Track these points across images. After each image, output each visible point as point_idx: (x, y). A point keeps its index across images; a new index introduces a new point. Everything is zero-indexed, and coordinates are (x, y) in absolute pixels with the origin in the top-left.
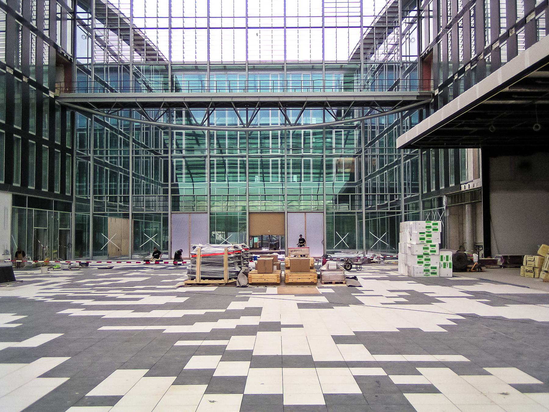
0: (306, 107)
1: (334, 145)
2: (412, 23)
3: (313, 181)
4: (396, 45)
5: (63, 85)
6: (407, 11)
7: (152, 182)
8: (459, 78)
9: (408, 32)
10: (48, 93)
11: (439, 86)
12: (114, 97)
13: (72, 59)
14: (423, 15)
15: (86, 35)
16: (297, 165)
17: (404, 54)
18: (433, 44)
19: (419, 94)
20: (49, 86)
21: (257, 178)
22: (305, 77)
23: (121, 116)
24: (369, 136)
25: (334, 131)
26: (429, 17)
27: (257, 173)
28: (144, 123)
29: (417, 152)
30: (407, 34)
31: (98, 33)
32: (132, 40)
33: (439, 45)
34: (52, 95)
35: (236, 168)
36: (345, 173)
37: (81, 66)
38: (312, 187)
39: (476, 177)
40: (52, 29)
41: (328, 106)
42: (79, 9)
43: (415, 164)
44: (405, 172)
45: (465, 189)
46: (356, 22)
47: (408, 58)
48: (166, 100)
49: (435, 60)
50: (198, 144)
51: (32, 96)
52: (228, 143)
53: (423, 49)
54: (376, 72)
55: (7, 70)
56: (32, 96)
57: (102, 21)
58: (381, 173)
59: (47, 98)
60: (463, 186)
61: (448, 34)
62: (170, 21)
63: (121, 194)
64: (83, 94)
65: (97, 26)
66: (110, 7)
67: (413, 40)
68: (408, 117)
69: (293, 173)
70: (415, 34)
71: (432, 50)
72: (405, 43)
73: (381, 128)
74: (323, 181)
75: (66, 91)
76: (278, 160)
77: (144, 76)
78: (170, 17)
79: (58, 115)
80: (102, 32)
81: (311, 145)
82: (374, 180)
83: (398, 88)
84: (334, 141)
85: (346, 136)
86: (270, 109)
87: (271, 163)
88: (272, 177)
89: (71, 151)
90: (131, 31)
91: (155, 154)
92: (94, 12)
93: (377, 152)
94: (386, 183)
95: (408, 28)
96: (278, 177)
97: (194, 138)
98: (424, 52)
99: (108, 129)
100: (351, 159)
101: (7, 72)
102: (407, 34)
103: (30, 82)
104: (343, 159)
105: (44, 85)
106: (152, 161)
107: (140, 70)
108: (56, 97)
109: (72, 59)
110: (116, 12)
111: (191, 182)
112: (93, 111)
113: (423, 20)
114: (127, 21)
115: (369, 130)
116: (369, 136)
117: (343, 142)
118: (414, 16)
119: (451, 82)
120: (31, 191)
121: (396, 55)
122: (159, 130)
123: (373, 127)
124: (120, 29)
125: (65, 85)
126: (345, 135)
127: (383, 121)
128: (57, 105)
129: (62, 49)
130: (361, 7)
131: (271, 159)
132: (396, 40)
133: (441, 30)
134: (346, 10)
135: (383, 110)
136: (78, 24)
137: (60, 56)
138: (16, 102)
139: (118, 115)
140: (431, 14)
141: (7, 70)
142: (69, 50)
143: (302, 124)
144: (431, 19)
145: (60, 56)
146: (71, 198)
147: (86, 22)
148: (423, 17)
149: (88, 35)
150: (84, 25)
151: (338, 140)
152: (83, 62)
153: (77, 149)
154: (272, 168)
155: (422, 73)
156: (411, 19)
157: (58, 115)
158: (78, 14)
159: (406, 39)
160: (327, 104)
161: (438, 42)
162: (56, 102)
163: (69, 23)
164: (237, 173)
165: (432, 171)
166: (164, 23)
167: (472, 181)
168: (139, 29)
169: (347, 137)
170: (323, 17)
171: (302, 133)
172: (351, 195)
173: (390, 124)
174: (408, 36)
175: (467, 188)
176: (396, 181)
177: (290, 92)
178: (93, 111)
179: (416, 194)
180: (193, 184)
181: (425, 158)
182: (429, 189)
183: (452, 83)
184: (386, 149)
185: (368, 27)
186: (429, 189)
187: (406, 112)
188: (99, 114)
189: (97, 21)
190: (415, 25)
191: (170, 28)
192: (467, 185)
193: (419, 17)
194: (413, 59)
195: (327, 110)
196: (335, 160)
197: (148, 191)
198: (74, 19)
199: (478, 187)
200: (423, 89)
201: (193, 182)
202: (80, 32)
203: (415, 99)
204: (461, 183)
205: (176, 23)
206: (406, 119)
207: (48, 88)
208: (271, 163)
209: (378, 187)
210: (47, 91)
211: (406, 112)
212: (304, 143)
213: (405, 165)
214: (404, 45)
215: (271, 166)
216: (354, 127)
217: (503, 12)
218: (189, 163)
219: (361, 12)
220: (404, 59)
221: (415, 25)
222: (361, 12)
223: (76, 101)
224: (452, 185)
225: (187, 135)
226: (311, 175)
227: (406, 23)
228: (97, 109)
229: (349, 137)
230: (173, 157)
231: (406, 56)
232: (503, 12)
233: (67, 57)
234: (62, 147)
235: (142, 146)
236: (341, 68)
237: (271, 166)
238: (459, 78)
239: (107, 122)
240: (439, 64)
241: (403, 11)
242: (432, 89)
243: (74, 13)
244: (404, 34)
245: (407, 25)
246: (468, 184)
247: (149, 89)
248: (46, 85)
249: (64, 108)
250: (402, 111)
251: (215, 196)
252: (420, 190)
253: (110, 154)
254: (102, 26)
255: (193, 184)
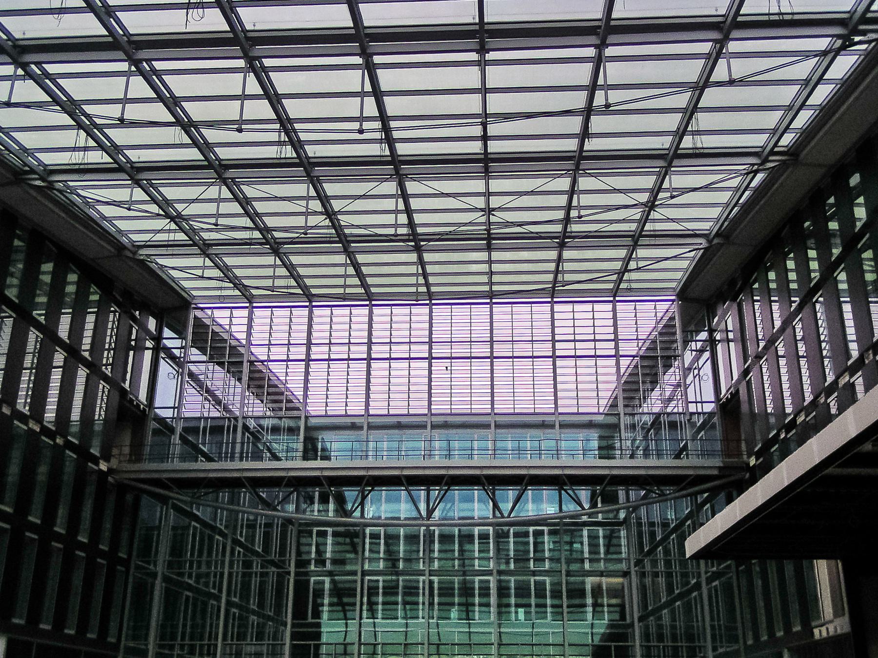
0: (527, 485)
1: (586, 555)
2: (701, 351)
3: (553, 621)
4: (678, 385)
5: (126, 450)
6: (691, 332)
7: (269, 618)
8: (788, 436)
9: (696, 364)
10: (97, 464)
11: (756, 449)
12: (526, 467)
13: (147, 409)
14: (718, 338)
15: (175, 372)
16: (523, 591)
17: (691, 398)
18: (739, 381)
19: (721, 465)
20: (101, 452)
21: (454, 613)
22: (530, 439)
23: (223, 502)
24: (646, 539)
25: (315, 529)
26: (728, 341)
27: (453, 604)
28: (262, 515)
29: (728, 567)
30: (695, 368)
31: (193, 368)
32: (245, 378)
33: (749, 383)
34: (103, 466)
35: (453, 595)
36: (609, 606)
37: (161, 421)
38: (551, 631)
39: (838, 613)
40: (120, 363)
41: (566, 484)
42: (167, 333)
43: (727, 588)
44: (710, 604)
45: (345, 640)
46: (607, 348)
47: (699, 405)
48: (371, 473)
49: (745, 408)
50: (355, 552)
51: (69, 468)
52: (405, 551)
53: (724, 391)
54: (649, 430)
55: (31, 425)
56: (69, 468)
57: (203, 350)
58: (658, 608)
59: (94, 471)
60: (816, 631)
61: (761, 368)
62: (370, 349)
63: (183, 639)
64: (154, 466)
65: (193, 358)
66: (217, 329)
67: (705, 378)
68: (708, 505)
69: (517, 606)
70: (707, 369)
71: (737, 391)
72: (693, 384)
73: (665, 525)
74: (563, 621)
75: (130, 461)
76: (378, 581)
77: (269, 438)
78: (370, 344)
79: (111, 500)
80: (202, 367)
81: (547, 554)
82: (660, 618)
83: (687, 455)
84: (586, 549)
85: (607, 540)
86: (457, 488)
87: (477, 586)
88: (479, 612)
89: (126, 563)
90: (246, 365)
91: (277, 569)
92: (190, 337)
93: (661, 566)
94: (680, 624)
95: (697, 359)
96: (490, 612)
97: (348, 540)
98: (725, 395)
99: (198, 526)
100: (620, 580)
101: (29, 427)
102: (695, 368)
103: (68, 445)
104: (604, 580)
105: (92, 451)
106: (272, 580)
107: (263, 429)
108: (111, 471)
109: (147, 409)
110: (225, 336)
111: (342, 620)
112: (171, 494)
113: (719, 347)
114: (242, 350)
115: (645, 529)
116: (646, 539)
117: (602, 550)
118: (704, 339)
119: (775, 445)
120: (44, 633)
121: (680, 402)
122: (288, 527)
123: (652, 524)
124: (228, 362)
125: (131, 451)
126: (604, 537)
127: (671, 515)
128: (112, 484)
129: (131, 394)
130: (615, 325)
131: (477, 579)
132: (678, 378)
133: (750, 361)
134: (571, 330)
135: (662, 491)
136: (163, 355)
137: (128, 405)
138: (65, 478)
139: (217, 500)
140: (731, 336)
141: (31, 425)
142: (143, 396)
143: (437, 518)
144: (732, 344)
145: (128, 405)
146: (116, 647)
147: (177, 352)
148: (719, 341)
149: (178, 372)
150: (173, 358)
151: (594, 547)
152: (167, 414)
153: (135, 561)
154: (480, 595)
155: (725, 431)
156: (699, 344)
157: (111, 500)
158: (164, 341)
159: (695, 377)
160: (564, 480)
161: (748, 378)
162: (110, 479)
163: (148, 355)
164: (397, 603)
165: (761, 604)
166: (422, 351)
167: (831, 622)
168: (262, 361)
169: (610, 541)
170: (554, 341)
171: (476, 533)
172: (615, 646)
173: (679, 518)
174: (696, 372)
175: (824, 634)
176: (697, 621)
177: (456, 461)
178: (171, 494)
179: (736, 647)
180: (346, 624)
181: (744, 582)
182: (756, 637)
183: (777, 446)
184: (238, 561)
185: (634, 356)
186: (756, 637)
187: (706, 495)
188: (181, 497)
189: (194, 351)
190: (707, 355)
191: (430, 358)
192: (824, 629)
193: (712, 343)
194: (709, 408)
195: (566, 491)
196: (590, 581)
197: (260, 636)
198: (158, 349)
199: (843, 632)
200: (729, 456)
201: (346, 619)
202: (165, 368)
203: (716, 472)
204: (813, 624)
205: (563, 349)
206: (705, 508)
207: (98, 455)
208: (477, 586)
209: (667, 631)
210: (95, 460)
211: (706, 495)
212: (535, 551)
213: (709, 591)
214: (692, 387)
215: (477, 592)
216: (620, 524)
217: (851, 332)
218: (341, 586)
219: (616, 332)
220: (692, 408)
221: (707, 355)
222: (616, 332)
223: (143, 476)
224: (797, 628)
225: (335, 534)
226: (549, 610)
227: (692, 351)
228: (177, 490)
229: (614, 541)
230: (461, 573)
231: (696, 402)
232: (851, 332)
233: (138, 406)
234: (112, 556)
235: (257, 554)
236: (590, 425)
237: (477, 592)
238: (788, 436)
239: (197, 513)
240: (752, 414)
241: (684, 331)
242: (745, 457)
243: (158, 338)
244: (689, 369)
245: (694, 353)
246: (827, 626)
247: (275, 457)
248: (95, 451)
249: (122, 488)
250: (695, 495)
251: (550, 645)
252: (741, 641)
253: (261, 568)
254: (204, 358)
255: (346, 624)
